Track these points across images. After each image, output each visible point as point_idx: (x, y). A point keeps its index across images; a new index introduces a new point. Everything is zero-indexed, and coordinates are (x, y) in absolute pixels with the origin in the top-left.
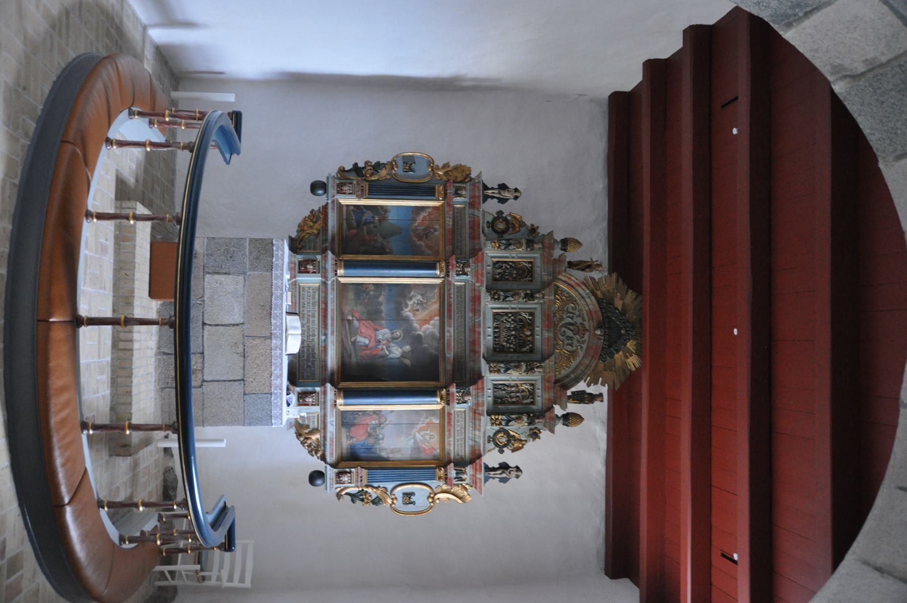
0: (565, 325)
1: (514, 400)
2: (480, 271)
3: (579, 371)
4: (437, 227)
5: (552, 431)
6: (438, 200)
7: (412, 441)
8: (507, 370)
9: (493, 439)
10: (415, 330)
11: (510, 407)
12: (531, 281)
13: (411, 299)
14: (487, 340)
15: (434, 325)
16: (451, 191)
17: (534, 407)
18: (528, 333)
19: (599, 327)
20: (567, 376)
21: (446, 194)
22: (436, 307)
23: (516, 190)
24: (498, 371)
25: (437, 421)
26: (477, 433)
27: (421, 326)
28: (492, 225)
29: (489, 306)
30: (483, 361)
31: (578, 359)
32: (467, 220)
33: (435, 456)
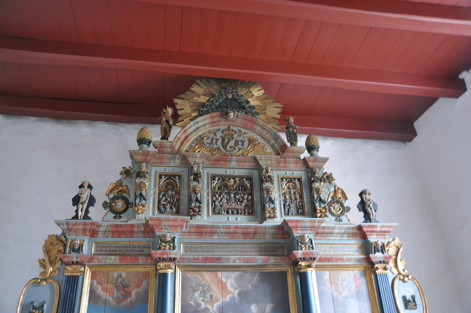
0: (224, 146)
1: (298, 197)
2: (171, 223)
3: (268, 136)
4: (116, 275)
5: (325, 160)
6: (84, 272)
7: (350, 300)
8: (272, 201)
9: (338, 218)
10: (233, 299)
11: (305, 200)
12: (180, 177)
13: (198, 305)
14: (242, 221)
15: (227, 278)
16: (74, 257)
17: (303, 178)
18: (232, 181)
19: (226, 115)
20: (273, 146)
21: (77, 263)
22: (207, 275)
23: (81, 186)
24: (274, 209)
25: (327, 273)
26: (336, 231)
27: (229, 292)
28: (118, 214)
29: (205, 218)
30: (265, 224)
31: (256, 137)
32: (110, 239)
33: (362, 275)
